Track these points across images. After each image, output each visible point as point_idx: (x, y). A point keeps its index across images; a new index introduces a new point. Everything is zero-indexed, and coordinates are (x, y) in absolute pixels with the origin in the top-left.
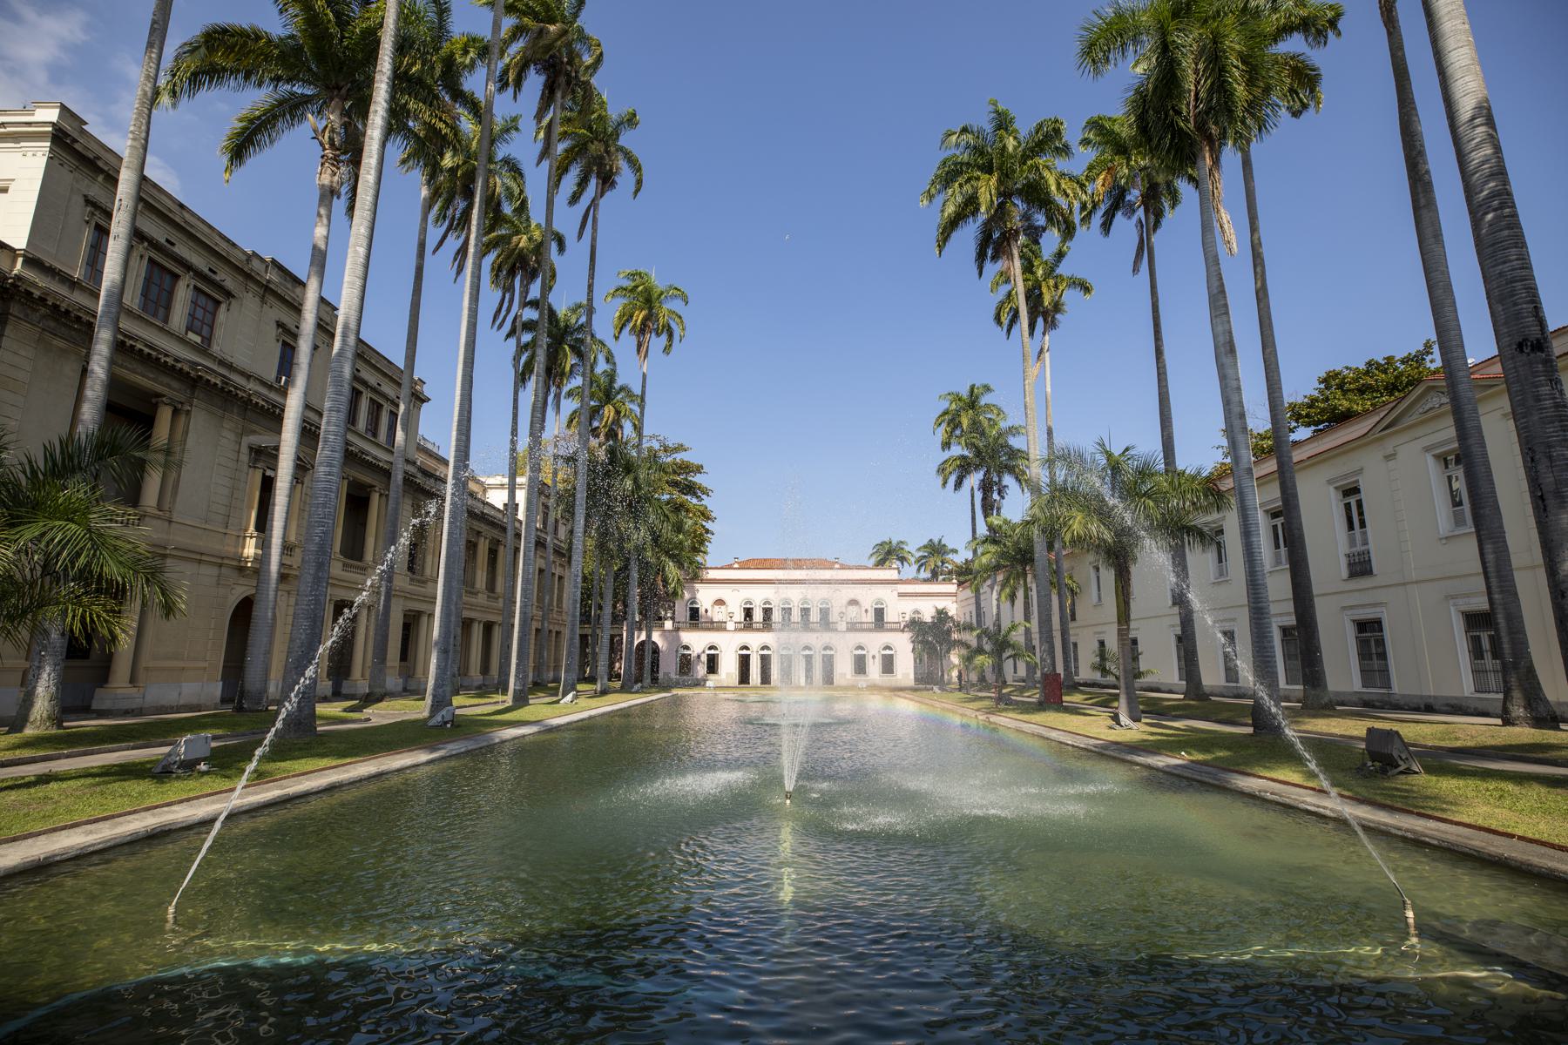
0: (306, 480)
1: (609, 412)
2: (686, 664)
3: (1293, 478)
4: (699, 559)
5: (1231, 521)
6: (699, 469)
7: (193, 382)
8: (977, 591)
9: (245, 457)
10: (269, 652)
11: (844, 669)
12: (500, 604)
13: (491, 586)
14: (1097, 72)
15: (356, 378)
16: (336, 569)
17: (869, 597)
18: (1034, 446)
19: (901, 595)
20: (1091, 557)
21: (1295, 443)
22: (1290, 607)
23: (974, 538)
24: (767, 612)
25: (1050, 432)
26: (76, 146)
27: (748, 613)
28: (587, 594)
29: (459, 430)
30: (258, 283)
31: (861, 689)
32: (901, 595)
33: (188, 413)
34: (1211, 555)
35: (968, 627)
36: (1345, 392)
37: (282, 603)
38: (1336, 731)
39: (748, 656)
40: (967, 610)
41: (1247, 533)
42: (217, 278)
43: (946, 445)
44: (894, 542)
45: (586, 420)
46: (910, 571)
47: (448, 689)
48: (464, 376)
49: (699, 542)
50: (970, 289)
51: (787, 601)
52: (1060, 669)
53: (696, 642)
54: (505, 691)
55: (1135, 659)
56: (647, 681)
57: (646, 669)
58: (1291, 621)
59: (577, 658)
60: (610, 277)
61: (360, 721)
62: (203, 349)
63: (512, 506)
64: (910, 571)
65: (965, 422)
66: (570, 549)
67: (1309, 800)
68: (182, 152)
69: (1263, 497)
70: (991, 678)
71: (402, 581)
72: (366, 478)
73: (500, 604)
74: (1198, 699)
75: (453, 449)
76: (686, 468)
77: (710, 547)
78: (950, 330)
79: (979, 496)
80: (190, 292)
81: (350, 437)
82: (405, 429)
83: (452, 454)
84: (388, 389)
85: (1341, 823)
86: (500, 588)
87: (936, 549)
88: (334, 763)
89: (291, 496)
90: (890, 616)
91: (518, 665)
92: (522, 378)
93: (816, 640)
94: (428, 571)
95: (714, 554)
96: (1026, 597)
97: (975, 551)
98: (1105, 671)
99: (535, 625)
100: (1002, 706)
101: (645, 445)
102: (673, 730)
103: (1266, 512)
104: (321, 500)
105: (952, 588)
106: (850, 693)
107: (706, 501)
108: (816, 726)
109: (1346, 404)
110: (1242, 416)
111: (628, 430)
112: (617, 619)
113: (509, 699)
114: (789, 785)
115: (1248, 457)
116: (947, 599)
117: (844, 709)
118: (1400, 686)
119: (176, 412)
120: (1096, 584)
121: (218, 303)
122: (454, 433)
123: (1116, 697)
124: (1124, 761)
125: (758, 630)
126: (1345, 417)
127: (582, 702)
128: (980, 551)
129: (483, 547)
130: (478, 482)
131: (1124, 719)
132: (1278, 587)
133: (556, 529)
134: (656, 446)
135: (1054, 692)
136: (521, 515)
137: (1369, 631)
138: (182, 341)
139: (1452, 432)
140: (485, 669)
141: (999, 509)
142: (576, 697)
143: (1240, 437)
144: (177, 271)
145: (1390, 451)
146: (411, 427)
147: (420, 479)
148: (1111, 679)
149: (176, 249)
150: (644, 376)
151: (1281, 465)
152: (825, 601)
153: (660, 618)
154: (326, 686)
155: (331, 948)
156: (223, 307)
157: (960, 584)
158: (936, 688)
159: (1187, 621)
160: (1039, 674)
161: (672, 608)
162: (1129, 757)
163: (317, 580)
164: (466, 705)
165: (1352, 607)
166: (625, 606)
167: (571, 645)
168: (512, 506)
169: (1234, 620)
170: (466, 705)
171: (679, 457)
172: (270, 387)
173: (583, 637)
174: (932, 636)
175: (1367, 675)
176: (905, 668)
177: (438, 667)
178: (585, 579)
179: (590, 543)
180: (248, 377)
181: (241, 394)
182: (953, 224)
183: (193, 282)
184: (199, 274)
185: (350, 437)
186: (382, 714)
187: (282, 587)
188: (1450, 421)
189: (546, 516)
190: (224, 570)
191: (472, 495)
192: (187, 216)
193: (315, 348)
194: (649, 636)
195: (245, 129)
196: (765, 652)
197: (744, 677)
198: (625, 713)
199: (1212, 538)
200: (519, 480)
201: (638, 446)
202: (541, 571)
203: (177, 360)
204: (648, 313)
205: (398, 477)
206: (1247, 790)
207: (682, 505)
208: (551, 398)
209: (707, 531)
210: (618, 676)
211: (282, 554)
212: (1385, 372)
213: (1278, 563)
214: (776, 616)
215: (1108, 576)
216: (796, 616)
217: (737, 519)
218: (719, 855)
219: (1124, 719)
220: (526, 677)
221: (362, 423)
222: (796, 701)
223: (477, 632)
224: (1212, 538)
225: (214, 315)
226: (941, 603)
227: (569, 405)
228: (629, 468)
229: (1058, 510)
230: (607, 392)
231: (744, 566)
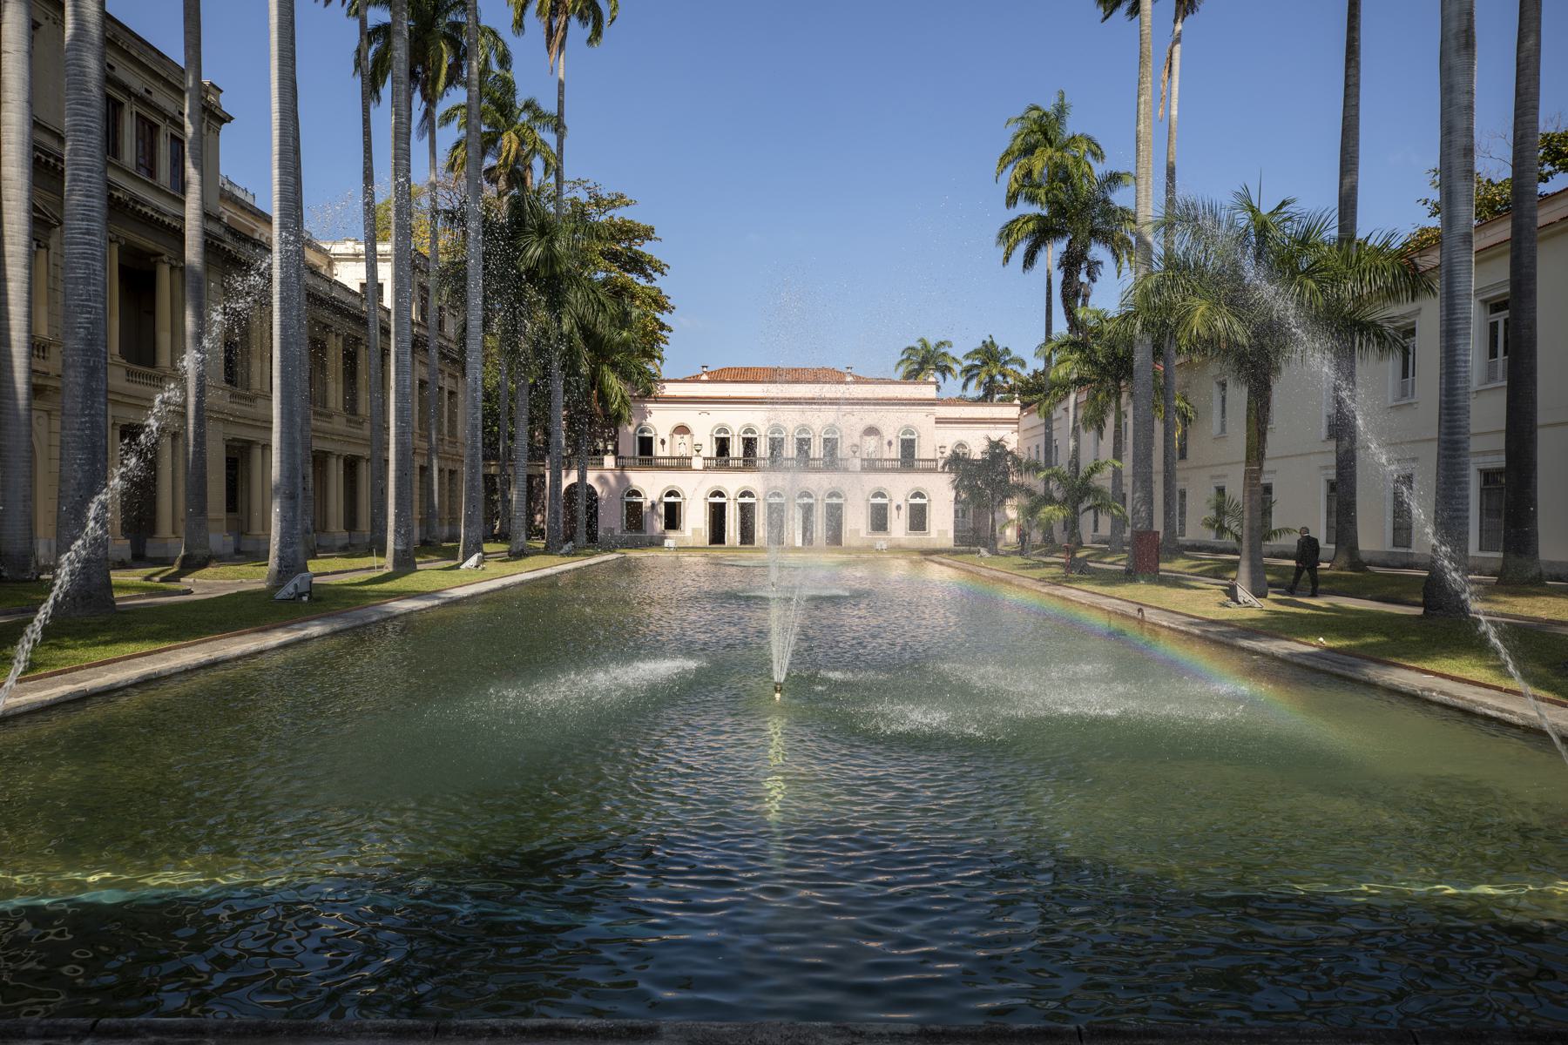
0: (53, 242)
1: (509, 141)
2: (634, 514)
3: (1534, 250)
4: (651, 367)
5: (1428, 314)
6: (647, 234)
8: (1048, 418)
10: (30, 498)
12: (366, 431)
13: (351, 406)
15: (109, 79)
16: (117, 378)
17: (893, 423)
18: (1143, 201)
19: (939, 421)
20: (1214, 368)
21: (1546, 198)
22: (1500, 442)
23: (1049, 340)
24: (749, 445)
25: (1171, 173)
28: (491, 416)
29: (282, 167)
32: (939, 421)
34: (1392, 364)
35: (1033, 467)
37: (41, 426)
38: (1543, 614)
39: (723, 505)
40: (1033, 443)
41: (1451, 332)
43: (1012, 200)
44: (932, 344)
46: (953, 386)
47: (300, 549)
48: (281, 79)
49: (650, 342)
51: (777, 428)
52: (1158, 526)
53: (650, 486)
54: (382, 552)
55: (1266, 512)
56: (582, 538)
57: (580, 523)
58: (1500, 462)
59: (481, 506)
61: (178, 593)
63: (372, 288)
64: (953, 386)
66: (462, 351)
67: (1490, 703)
69: (1482, 279)
70: (1060, 536)
71: (219, 397)
72: (148, 243)
73: (366, 431)
75: (276, 197)
76: (628, 232)
77: (667, 351)
79: (1058, 277)
81: (114, 176)
82: (199, 165)
83: (276, 204)
84: (161, 98)
85: (1533, 733)
86: (363, 408)
87: (990, 355)
88: (174, 644)
89: (31, 266)
90: (924, 451)
91: (397, 516)
92: (371, 89)
93: (818, 482)
94: (256, 383)
95: (673, 359)
96: (1118, 426)
97: (1048, 359)
98: (1221, 530)
99: (418, 461)
100: (1075, 575)
101: (567, 196)
103: (1484, 302)
104: (80, 273)
105: (1012, 412)
108: (818, 601)
110: (1469, 151)
111: (537, 176)
112: (537, 454)
113: (387, 563)
114: (779, 676)
115: (1467, 215)
116: (1003, 427)
117: (858, 576)
120: (1220, 409)
122: (276, 172)
123: (1234, 565)
124: (1232, 647)
125: (737, 469)
127: (492, 567)
128: (1055, 358)
129: (335, 348)
130: (319, 250)
131: (1243, 594)
132: (1487, 414)
133: (441, 324)
134: (583, 197)
135: (1147, 557)
136: (388, 301)
140: (351, 522)
141: (1086, 296)
142: (482, 560)
143: (1460, 186)
146: (209, 165)
147: (230, 244)
148: (1228, 540)
150: (561, 84)
151: (1517, 230)
153: (597, 452)
154: (121, 546)
155: (171, 879)
158: (983, 551)
159: (1346, 465)
160: (1128, 534)
162: (1246, 643)
163: (90, 393)
164: (331, 570)
166: (547, 433)
167: (472, 488)
168: (372, 288)
170: (331, 570)
171: (619, 214)
173: (489, 479)
174: (981, 479)
176: (942, 525)
177: (283, 519)
178: (488, 397)
179: (492, 343)
185: (114, 176)
187: (37, 404)
188: (1507, 260)
189: (424, 300)
191: (314, 271)
193: (34, 26)
194: (582, 477)
196: (747, 500)
197: (717, 534)
198: (550, 582)
199: (1400, 341)
200: (380, 248)
201: (556, 198)
202: (423, 384)
206: (1405, 688)
207: (624, 288)
209: (662, 327)
210: (541, 532)
211: (30, 356)
213: (1491, 377)
214: (762, 449)
215: (1239, 396)
217: (701, 311)
218: (691, 749)
219: (1243, 594)
220: (409, 533)
221: (129, 154)
222: (792, 566)
223: (336, 472)
224: (1400, 341)
226: (996, 434)
227: (449, 135)
228: (545, 230)
230: (500, 103)
231: (716, 378)
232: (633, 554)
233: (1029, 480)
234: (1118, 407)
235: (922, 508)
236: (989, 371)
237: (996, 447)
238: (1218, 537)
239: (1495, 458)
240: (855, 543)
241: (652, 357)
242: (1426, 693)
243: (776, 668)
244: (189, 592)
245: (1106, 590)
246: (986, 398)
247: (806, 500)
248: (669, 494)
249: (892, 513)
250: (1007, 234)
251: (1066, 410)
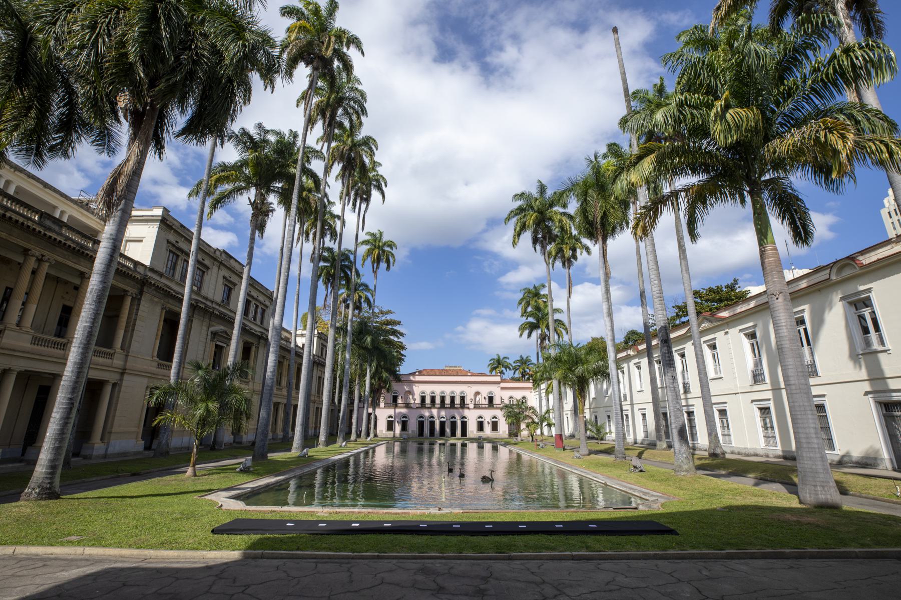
9: (209, 337)
17: (485, 390)
19: (502, 388)
30: (218, 261)
32: (502, 388)
39: (423, 422)
64: (509, 374)
90: (497, 401)
100: (397, 448)
105: (530, 385)
171: (389, 317)
172: (220, 305)
205: (293, 352)
209: (403, 355)
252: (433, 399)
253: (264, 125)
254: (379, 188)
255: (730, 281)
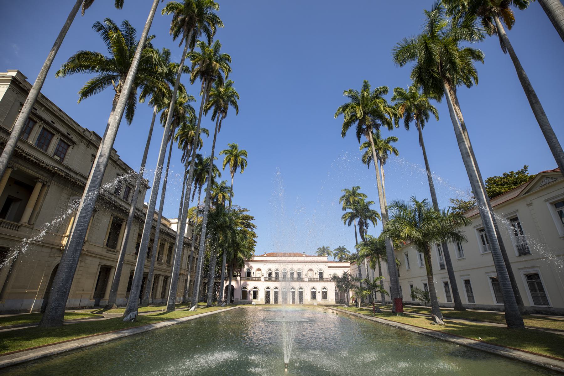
2: (245, 294)
6: (252, 218)
7: (53, 174)
11: (307, 297)
14: (401, 65)
17: (317, 268)
19: (329, 267)
22: (494, 269)
24: (277, 274)
26: (21, 85)
27: (270, 275)
30: (86, 140)
31: (315, 306)
32: (329, 267)
33: (49, 186)
35: (356, 280)
36: (497, 185)
38: (538, 325)
39: (269, 292)
42: (70, 137)
45: (211, 198)
49: (251, 247)
50: (353, 147)
51: (285, 269)
60: (223, 145)
62: (60, 163)
65: (351, 200)
68: (65, 93)
72: (121, 216)
74: (460, 310)
77: (255, 248)
78: (346, 164)
79: (358, 228)
80: (58, 141)
87: (341, 250)
90: (325, 276)
95: (258, 249)
97: (357, 250)
102: (241, 322)
105: (348, 264)
106: (310, 307)
107: (255, 230)
109: (498, 189)
116: (343, 269)
118: (553, 303)
119: (44, 185)
121: (69, 146)
126: (499, 194)
127: (199, 310)
128: (359, 249)
129: (167, 245)
137: (533, 279)
138: (51, 158)
139: (481, 222)
141: (366, 232)
144: (54, 132)
145: (529, 202)
149: (55, 125)
152: (299, 269)
156: (71, 147)
157: (351, 263)
161: (240, 272)
162: (452, 340)
165: (523, 268)
169: (469, 275)
171: (244, 213)
174: (343, 283)
175: (535, 299)
176: (332, 298)
180: (77, 174)
181: (72, 180)
182: (347, 125)
183: (60, 137)
184: (63, 135)
186: (109, 315)
190: (53, 250)
192: (62, 114)
194: (230, 283)
195: (89, 86)
196: (276, 290)
197: (268, 301)
202: (189, 256)
203: (47, 165)
204: (237, 161)
207: (245, 232)
208: (197, 189)
209: (255, 242)
212: (511, 177)
213: (485, 250)
214: (281, 276)
216: (288, 275)
217: (265, 237)
222: (287, 309)
223: (161, 280)
225: (67, 150)
228: (225, 215)
229: (397, 225)
231: (268, 255)
232: (244, 306)
233: (357, 284)
234: (379, 262)
235: (326, 292)
236: (341, 255)
237: (345, 274)
238: (413, 300)
239: (494, 274)
240: (307, 303)
241: (251, 250)
242: (547, 366)
243: (285, 357)
244: (103, 317)
245: (386, 318)
246: (341, 261)
247: (293, 290)
248: (255, 288)
249: (317, 294)
250: (343, 217)
251: (364, 263)
252: (277, 274)
253: (130, 23)
254: (234, 103)
255: (521, 168)
